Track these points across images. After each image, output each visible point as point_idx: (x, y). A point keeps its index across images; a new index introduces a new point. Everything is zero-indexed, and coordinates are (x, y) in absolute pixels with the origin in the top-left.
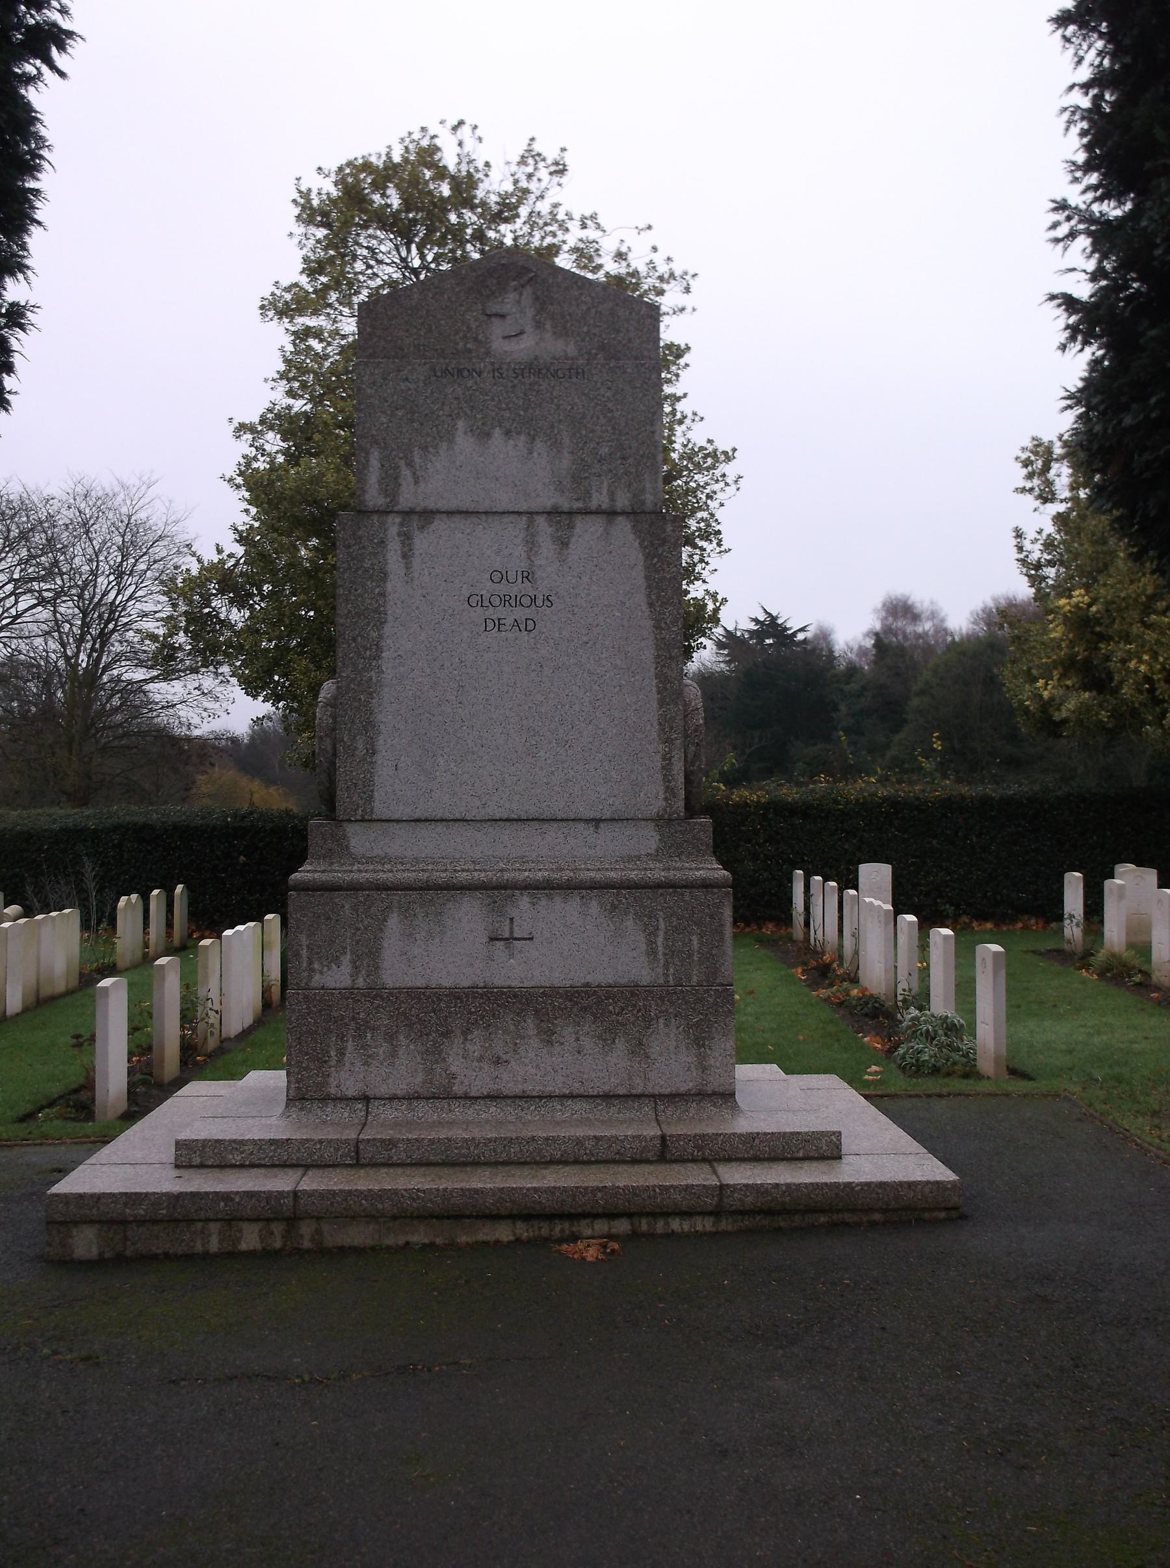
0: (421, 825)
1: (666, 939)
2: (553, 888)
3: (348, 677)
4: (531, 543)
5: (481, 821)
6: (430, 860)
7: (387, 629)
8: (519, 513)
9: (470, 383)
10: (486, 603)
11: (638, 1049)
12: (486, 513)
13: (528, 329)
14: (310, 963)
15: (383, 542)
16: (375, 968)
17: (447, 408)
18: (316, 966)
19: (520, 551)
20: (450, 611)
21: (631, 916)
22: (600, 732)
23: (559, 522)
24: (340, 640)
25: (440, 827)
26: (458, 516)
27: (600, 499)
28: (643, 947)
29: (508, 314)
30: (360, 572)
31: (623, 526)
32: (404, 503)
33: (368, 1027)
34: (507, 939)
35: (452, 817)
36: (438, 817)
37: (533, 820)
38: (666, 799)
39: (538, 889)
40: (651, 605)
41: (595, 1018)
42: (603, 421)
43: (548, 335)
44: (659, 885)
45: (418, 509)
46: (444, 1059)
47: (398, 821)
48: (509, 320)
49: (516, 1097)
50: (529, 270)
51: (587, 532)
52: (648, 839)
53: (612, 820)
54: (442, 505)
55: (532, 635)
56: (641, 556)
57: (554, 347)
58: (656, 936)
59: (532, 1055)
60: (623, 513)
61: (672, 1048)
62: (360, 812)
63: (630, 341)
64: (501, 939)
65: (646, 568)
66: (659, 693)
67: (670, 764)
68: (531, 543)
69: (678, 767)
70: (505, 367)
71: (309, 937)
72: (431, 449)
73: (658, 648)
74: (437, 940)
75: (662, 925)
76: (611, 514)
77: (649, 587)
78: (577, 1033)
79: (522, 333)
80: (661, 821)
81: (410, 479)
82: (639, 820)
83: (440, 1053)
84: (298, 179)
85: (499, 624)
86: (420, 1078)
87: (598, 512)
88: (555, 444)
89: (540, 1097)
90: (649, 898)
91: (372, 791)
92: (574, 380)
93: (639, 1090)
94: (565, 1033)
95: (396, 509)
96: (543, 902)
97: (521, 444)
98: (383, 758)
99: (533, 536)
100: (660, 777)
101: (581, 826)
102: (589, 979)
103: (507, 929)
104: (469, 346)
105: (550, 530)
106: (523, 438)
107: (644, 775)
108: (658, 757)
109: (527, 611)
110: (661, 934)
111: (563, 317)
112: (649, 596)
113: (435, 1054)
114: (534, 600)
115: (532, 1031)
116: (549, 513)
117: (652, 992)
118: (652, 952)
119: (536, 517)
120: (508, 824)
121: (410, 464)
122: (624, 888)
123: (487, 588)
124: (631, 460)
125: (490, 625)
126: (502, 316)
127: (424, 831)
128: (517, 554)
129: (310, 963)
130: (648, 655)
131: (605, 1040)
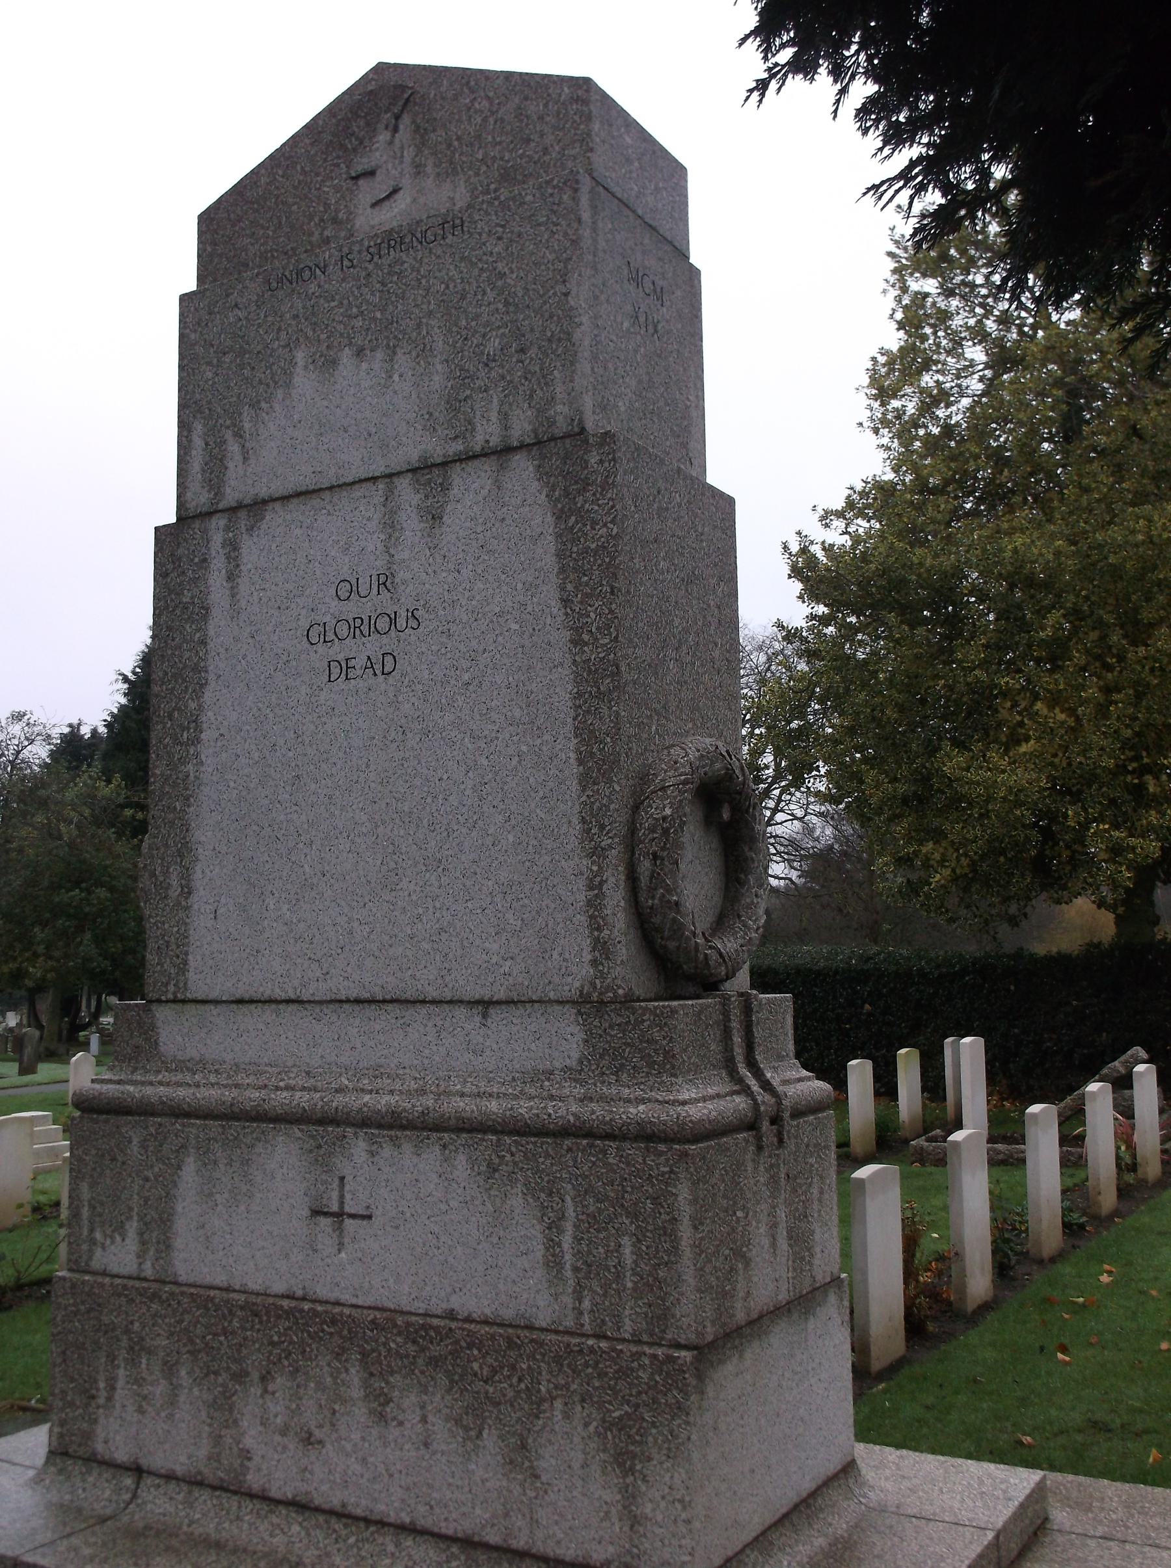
0: (244, 1009)
1: (578, 1240)
2: (403, 1128)
3: (162, 775)
4: (391, 526)
5: (321, 1002)
6: (252, 1068)
7: (208, 696)
8: (374, 479)
9: (312, 288)
10: (330, 636)
11: (520, 1455)
12: (331, 488)
13: (406, 182)
14: (92, 1230)
15: (205, 560)
16: (165, 1246)
17: (283, 335)
18: (98, 1235)
19: (374, 543)
20: (285, 658)
21: (520, 1188)
22: (489, 841)
23: (429, 481)
24: (155, 719)
25: (268, 1013)
26: (295, 501)
27: (487, 432)
28: (539, 1253)
29: (378, 167)
30: (178, 612)
31: (523, 467)
32: (231, 497)
33: (142, 1349)
34: (333, 1215)
35: (284, 996)
36: (266, 996)
37: (392, 1001)
38: (594, 963)
39: (380, 1126)
40: (566, 602)
41: (452, 1381)
42: (491, 295)
43: (429, 182)
44: (564, 1132)
45: (247, 501)
46: (235, 1421)
47: (216, 1002)
48: (379, 176)
49: (331, 1512)
50: (403, 88)
51: (470, 488)
52: (565, 1039)
53: (509, 1002)
54: (277, 487)
55: (391, 680)
56: (550, 519)
57: (448, 195)
58: (560, 1231)
59: (356, 1436)
60: (522, 447)
61: (576, 1465)
62: (171, 988)
63: (546, 151)
64: (326, 1214)
65: (559, 536)
66: (581, 762)
67: (601, 895)
68: (391, 526)
69: (616, 898)
70: (356, 248)
71: (91, 1187)
72: (263, 405)
73: (578, 679)
74: (243, 1208)
75: (570, 1212)
76: (505, 451)
77: (562, 570)
78: (423, 1407)
79: (395, 191)
80: (590, 1005)
81: (238, 457)
82: (550, 1001)
83: (231, 1410)
84: (892, 229)
85: (346, 667)
86: (203, 1453)
87: (484, 454)
88: (424, 352)
89: (367, 1521)
90: (547, 1155)
91: (187, 954)
92: (450, 239)
93: (519, 1543)
94: (406, 1403)
95: (221, 506)
96: (387, 1151)
97: (377, 366)
98: (201, 900)
99: (393, 513)
100: (581, 919)
101: (461, 1012)
102: (456, 1303)
103: (335, 1195)
104: (327, 233)
105: (416, 499)
106: (379, 355)
107: (559, 917)
108: (581, 883)
109: (385, 639)
110: (569, 1227)
111: (449, 146)
112: (563, 588)
113: (223, 1408)
114: (393, 621)
115: (356, 1392)
116: (413, 471)
117: (541, 1344)
118: (553, 1262)
119: (395, 480)
120: (357, 1008)
121: (238, 435)
122: (511, 1133)
123: (331, 609)
124: (533, 352)
125: (336, 671)
126: (371, 173)
127: (251, 1020)
128: (371, 547)
129: (92, 1230)
130: (563, 694)
131: (467, 1429)
